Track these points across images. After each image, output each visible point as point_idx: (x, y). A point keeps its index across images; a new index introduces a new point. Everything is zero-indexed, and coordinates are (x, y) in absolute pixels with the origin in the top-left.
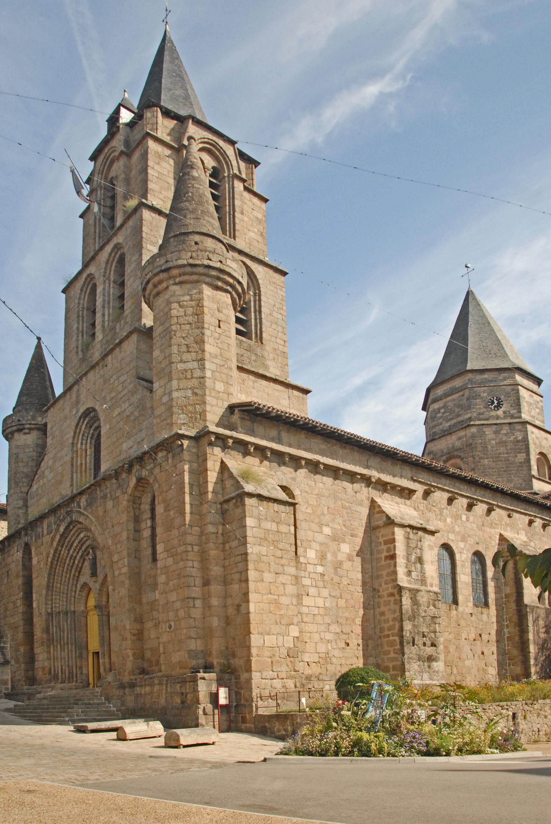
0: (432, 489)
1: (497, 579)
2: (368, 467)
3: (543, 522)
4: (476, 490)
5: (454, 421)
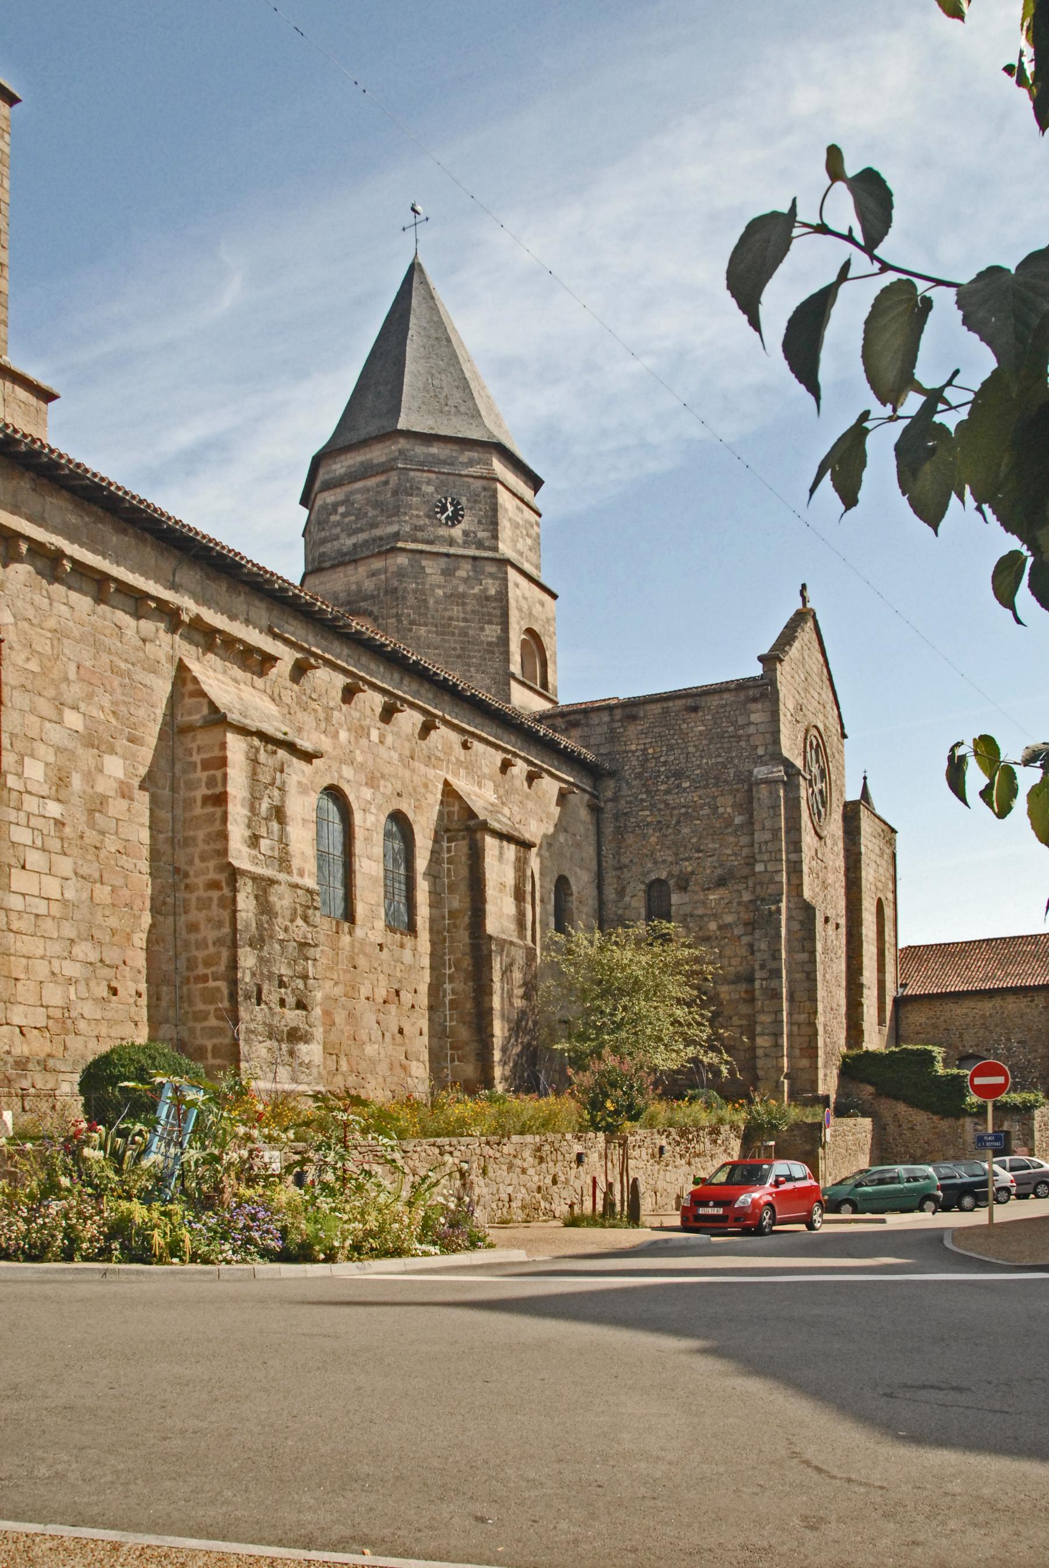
0: (312, 661)
1: (435, 877)
2: (174, 587)
3: (530, 768)
4: (402, 680)
5: (362, 537)
